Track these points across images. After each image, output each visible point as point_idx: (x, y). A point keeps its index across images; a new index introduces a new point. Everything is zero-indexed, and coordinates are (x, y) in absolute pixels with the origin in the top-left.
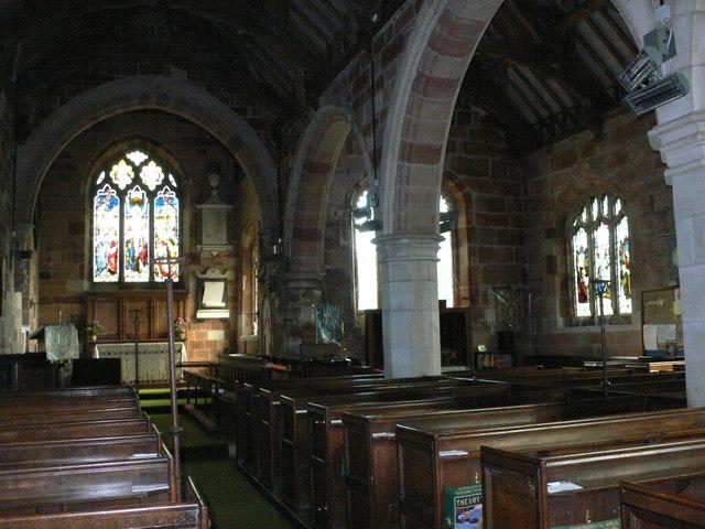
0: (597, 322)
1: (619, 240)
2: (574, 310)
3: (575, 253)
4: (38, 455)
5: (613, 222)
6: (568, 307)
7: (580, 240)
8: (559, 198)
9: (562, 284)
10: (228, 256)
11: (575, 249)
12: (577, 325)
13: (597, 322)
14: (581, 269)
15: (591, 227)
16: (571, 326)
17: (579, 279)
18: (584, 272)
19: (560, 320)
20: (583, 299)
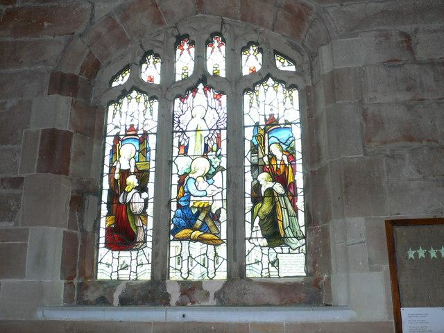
0: (175, 296)
1: (248, 121)
2: (94, 264)
3: (109, 141)
4: (231, 87)
5: (235, 87)
6: (78, 260)
7: (130, 114)
8: (109, 17)
9: (73, 198)
10: (170, 305)
11: (111, 130)
12: (104, 301)
13: (175, 296)
14: (125, 174)
15: (168, 93)
16: (83, 303)
17: (113, 195)
18: (132, 180)
19: (55, 282)
20: (123, 238)
